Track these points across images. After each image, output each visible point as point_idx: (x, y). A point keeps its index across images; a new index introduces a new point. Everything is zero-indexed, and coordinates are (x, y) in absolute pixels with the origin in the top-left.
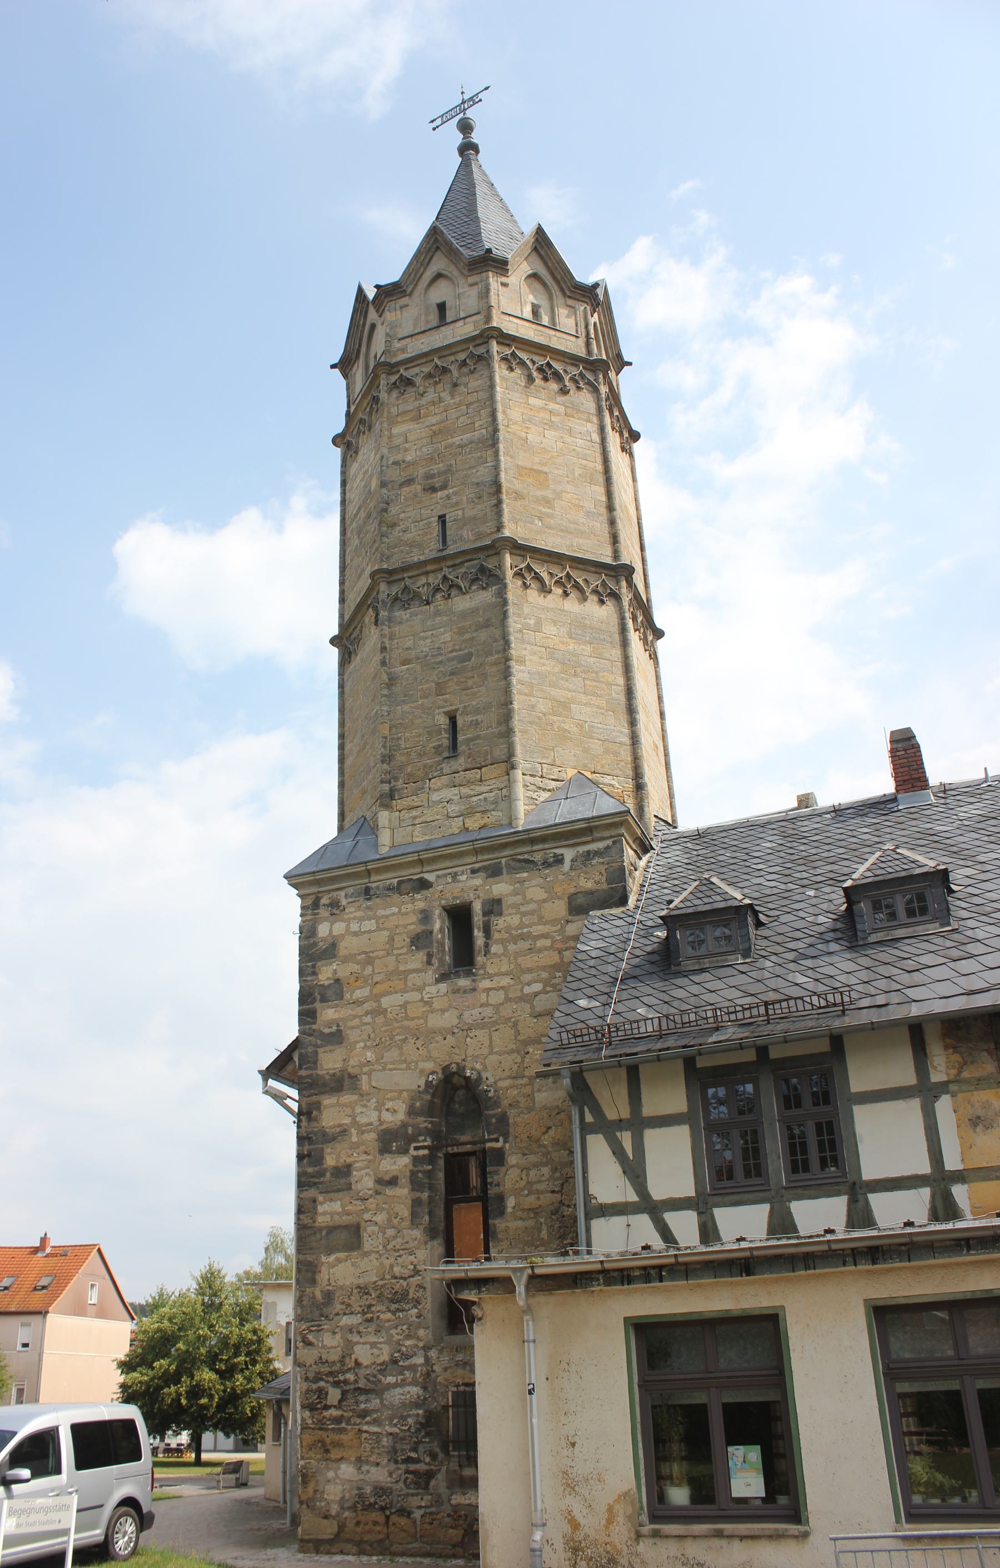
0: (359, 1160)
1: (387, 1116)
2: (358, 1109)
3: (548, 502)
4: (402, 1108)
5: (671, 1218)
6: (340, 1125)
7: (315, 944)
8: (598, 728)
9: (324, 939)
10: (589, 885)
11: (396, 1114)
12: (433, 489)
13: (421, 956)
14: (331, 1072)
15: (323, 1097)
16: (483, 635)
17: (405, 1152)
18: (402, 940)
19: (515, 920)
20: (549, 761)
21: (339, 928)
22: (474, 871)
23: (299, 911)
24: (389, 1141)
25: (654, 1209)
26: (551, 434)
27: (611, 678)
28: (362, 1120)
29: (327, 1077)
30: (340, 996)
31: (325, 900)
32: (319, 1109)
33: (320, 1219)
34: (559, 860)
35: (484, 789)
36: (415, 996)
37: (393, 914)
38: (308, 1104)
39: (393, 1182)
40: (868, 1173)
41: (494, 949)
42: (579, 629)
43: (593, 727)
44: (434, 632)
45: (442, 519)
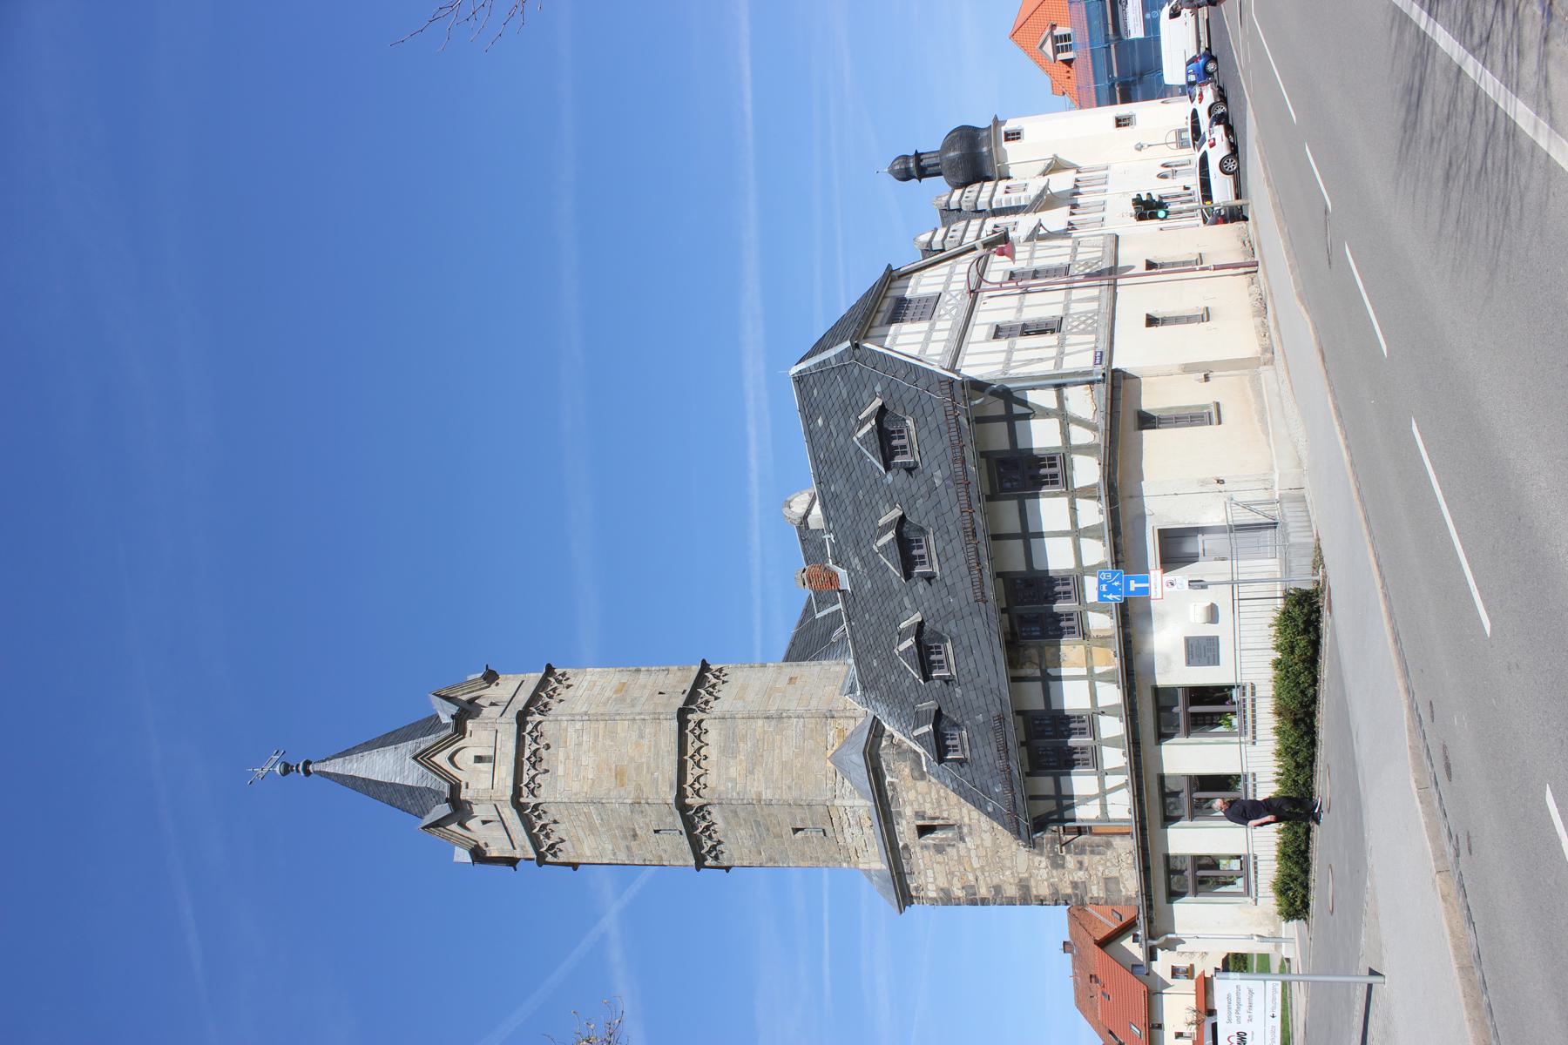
0: (1068, 878)
1: (1043, 865)
4: (1038, 858)
10: (907, 770)
11: (1042, 862)
12: (635, 836)
13: (949, 849)
16: (742, 814)
18: (939, 858)
19: (928, 806)
21: (930, 887)
24: (1057, 863)
25: (1103, 793)
27: (759, 730)
30: (972, 887)
34: (892, 784)
36: (973, 853)
39: (1081, 863)
42: (728, 750)
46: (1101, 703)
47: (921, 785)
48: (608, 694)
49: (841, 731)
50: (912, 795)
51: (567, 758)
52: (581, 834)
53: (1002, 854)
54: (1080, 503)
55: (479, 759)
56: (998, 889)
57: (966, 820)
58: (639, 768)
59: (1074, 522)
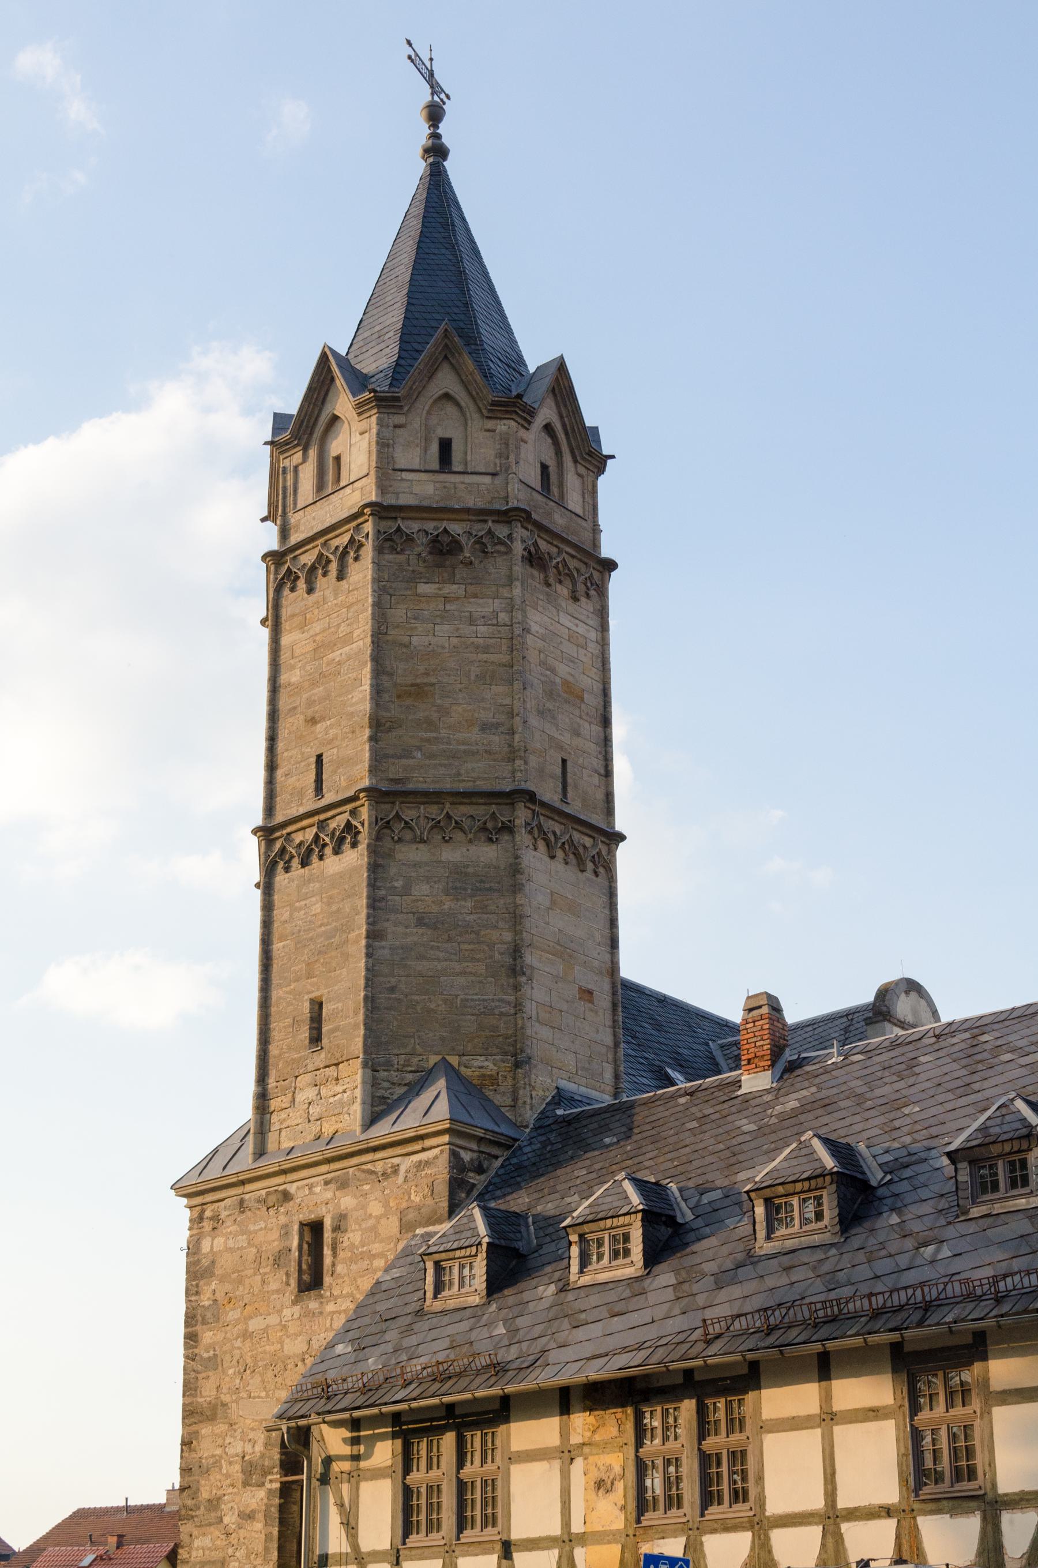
2: (228, 1440)
3: (430, 725)
5: (345, 1548)
6: (213, 1456)
7: (199, 1261)
8: (472, 1000)
9: (206, 1256)
12: (313, 721)
14: (208, 1399)
15: (201, 1425)
17: (262, 1485)
20: (407, 1050)
21: (219, 1242)
22: (327, 1183)
23: (188, 1224)
26: (443, 629)
28: (231, 1451)
29: (205, 1405)
31: (208, 1214)
32: (197, 1439)
33: (194, 1554)
34: (396, 1170)
35: (339, 1088)
36: (273, 1320)
37: (261, 1229)
38: (188, 1433)
40: (774, 1507)
41: (340, 1268)
42: (461, 882)
43: (467, 1000)
44: (307, 902)
45: (319, 758)
46: (779, 1538)
47: (391, 1225)
48: (563, 670)
49: (494, 1080)
50: (375, 1208)
51: (447, 599)
52: (317, 627)
53: (718, 1330)
54: (889, 1526)
55: (445, 446)
56: (213, 1363)
57: (330, 1307)
58: (430, 725)
59: (854, 1514)
